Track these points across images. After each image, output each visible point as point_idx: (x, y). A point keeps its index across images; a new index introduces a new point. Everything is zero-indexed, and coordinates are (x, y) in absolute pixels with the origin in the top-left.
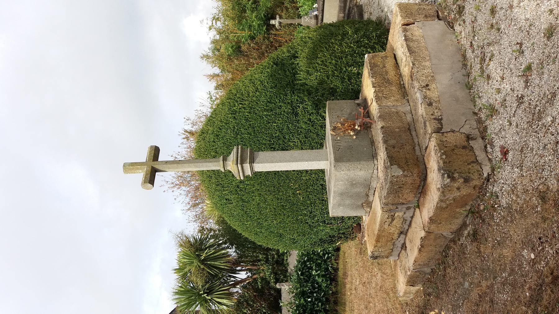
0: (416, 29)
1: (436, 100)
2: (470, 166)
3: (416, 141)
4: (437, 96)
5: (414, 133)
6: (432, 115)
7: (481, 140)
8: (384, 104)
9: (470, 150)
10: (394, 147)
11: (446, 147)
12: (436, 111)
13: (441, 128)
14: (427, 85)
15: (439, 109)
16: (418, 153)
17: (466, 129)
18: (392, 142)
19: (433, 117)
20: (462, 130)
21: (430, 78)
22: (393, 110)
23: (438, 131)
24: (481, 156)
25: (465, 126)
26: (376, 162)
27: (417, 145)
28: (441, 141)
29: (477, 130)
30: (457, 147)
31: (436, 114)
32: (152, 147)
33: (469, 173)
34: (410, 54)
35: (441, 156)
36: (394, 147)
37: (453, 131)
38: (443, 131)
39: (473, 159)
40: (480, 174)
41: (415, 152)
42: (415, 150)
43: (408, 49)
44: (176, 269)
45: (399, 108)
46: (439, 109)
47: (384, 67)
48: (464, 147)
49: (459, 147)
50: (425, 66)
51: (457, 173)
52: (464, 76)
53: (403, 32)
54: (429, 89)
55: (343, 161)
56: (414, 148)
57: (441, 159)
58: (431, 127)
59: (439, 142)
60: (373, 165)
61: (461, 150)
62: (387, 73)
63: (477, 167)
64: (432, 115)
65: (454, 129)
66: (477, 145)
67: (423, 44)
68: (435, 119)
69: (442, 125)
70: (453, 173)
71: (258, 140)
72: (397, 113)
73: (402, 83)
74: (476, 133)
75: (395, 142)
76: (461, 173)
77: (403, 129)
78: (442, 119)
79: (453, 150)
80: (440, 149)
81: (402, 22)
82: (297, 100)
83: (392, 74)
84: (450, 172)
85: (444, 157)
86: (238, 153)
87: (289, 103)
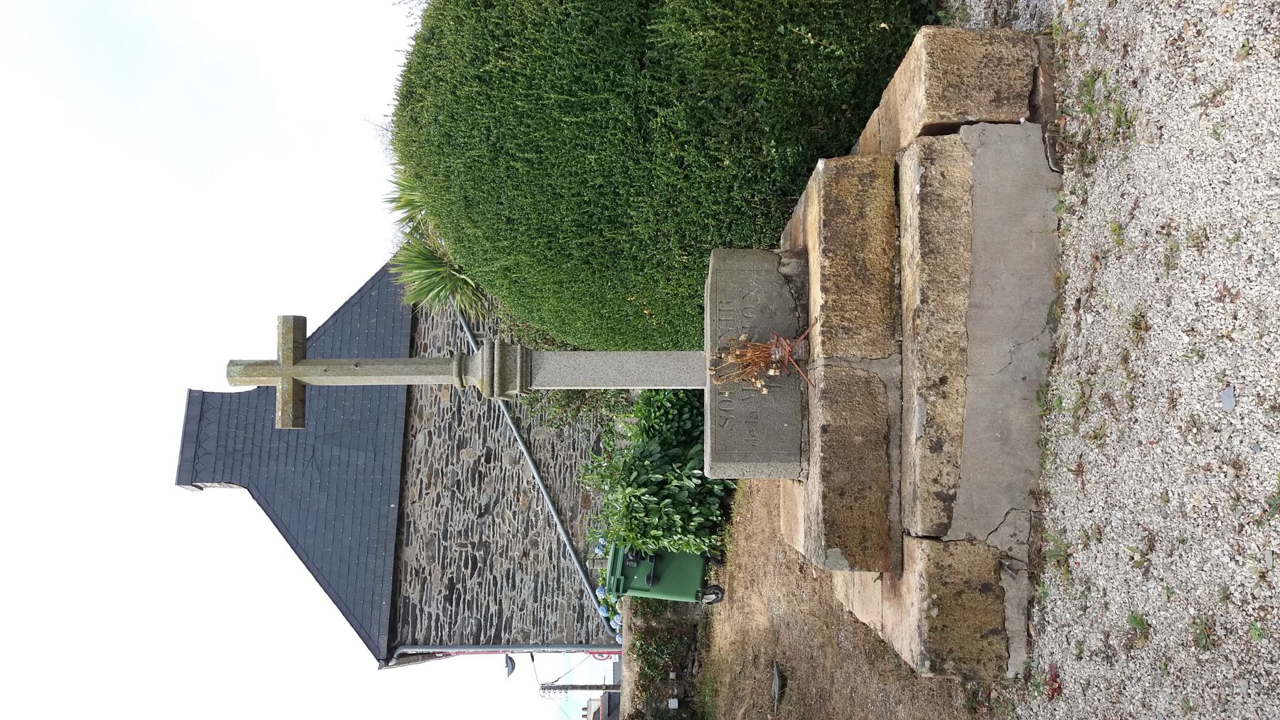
0: (958, 152)
1: (955, 432)
2: (985, 643)
3: (895, 477)
4: (959, 419)
5: (895, 453)
6: (935, 481)
7: (1026, 581)
8: (841, 354)
9: (998, 597)
10: (842, 495)
11: (945, 584)
12: (945, 470)
13: (945, 528)
14: (943, 381)
15: (956, 466)
16: (893, 514)
17: (1001, 541)
18: (840, 477)
19: (937, 488)
20: (994, 540)
21: (954, 355)
22: (859, 373)
23: (936, 536)
24: (1015, 624)
25: (1002, 530)
26: (805, 465)
27: (895, 491)
28: (938, 566)
29: (1025, 547)
30: (969, 587)
31: (944, 480)
32: (285, 319)
33: (978, 662)
34: (923, 256)
35: (929, 609)
36: (842, 495)
37: (972, 540)
38: (951, 535)
39: (996, 624)
40: (1000, 667)
41: (887, 511)
42: (888, 504)
43: (922, 238)
44: (393, 200)
45: (875, 368)
46: (956, 466)
47: (862, 215)
48: (985, 588)
49: (974, 585)
50: (950, 308)
51: (953, 659)
52: (1042, 354)
53: (921, 164)
54: (944, 396)
55: (732, 460)
56: (887, 497)
57: (928, 617)
58: (923, 519)
59: (933, 570)
60: (799, 469)
61: (977, 594)
62: (865, 238)
63: (999, 647)
64: (935, 481)
65: (975, 533)
66: (1015, 588)
67: (965, 220)
68: (939, 495)
69: (950, 518)
70: (944, 660)
71: (550, 185)
72: (868, 382)
73: (897, 282)
74: (1021, 552)
75: (848, 475)
76: (960, 659)
77: (873, 437)
78: (953, 497)
79: (959, 593)
80: (932, 590)
81: (926, 121)
82: (651, 92)
83: (874, 252)
84: (937, 656)
85: (935, 612)
86: (492, 369)
87: (628, 98)
